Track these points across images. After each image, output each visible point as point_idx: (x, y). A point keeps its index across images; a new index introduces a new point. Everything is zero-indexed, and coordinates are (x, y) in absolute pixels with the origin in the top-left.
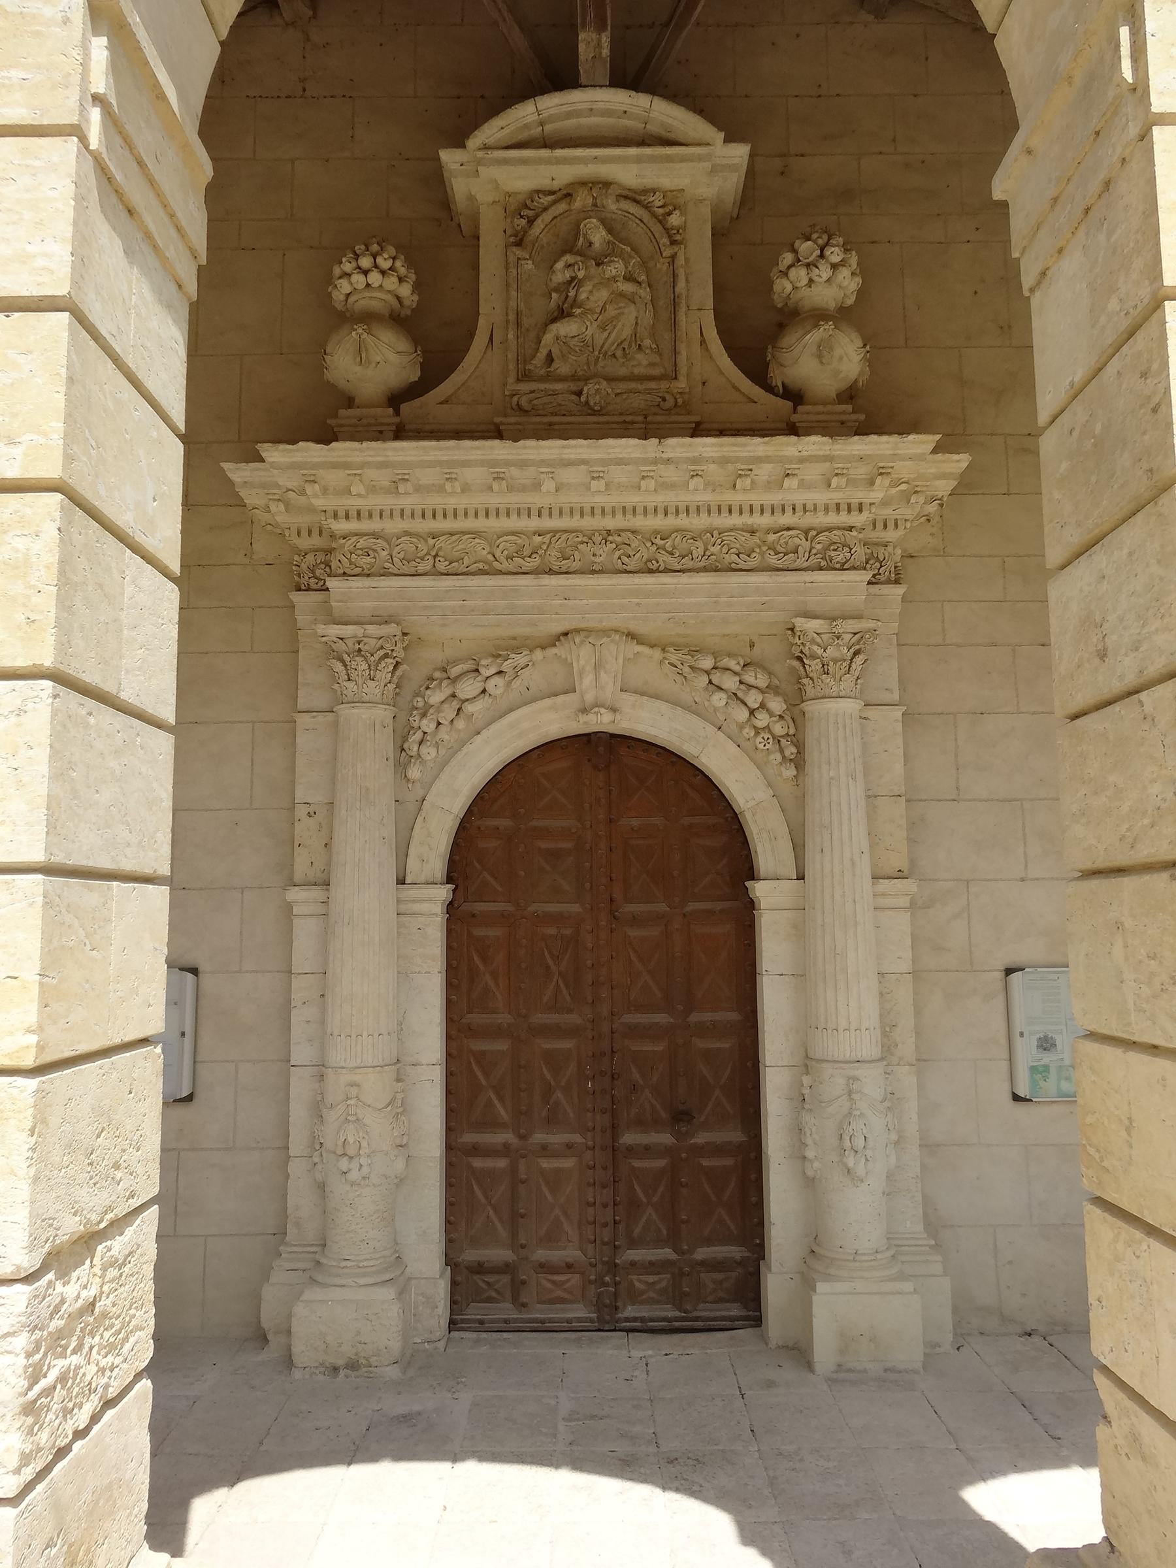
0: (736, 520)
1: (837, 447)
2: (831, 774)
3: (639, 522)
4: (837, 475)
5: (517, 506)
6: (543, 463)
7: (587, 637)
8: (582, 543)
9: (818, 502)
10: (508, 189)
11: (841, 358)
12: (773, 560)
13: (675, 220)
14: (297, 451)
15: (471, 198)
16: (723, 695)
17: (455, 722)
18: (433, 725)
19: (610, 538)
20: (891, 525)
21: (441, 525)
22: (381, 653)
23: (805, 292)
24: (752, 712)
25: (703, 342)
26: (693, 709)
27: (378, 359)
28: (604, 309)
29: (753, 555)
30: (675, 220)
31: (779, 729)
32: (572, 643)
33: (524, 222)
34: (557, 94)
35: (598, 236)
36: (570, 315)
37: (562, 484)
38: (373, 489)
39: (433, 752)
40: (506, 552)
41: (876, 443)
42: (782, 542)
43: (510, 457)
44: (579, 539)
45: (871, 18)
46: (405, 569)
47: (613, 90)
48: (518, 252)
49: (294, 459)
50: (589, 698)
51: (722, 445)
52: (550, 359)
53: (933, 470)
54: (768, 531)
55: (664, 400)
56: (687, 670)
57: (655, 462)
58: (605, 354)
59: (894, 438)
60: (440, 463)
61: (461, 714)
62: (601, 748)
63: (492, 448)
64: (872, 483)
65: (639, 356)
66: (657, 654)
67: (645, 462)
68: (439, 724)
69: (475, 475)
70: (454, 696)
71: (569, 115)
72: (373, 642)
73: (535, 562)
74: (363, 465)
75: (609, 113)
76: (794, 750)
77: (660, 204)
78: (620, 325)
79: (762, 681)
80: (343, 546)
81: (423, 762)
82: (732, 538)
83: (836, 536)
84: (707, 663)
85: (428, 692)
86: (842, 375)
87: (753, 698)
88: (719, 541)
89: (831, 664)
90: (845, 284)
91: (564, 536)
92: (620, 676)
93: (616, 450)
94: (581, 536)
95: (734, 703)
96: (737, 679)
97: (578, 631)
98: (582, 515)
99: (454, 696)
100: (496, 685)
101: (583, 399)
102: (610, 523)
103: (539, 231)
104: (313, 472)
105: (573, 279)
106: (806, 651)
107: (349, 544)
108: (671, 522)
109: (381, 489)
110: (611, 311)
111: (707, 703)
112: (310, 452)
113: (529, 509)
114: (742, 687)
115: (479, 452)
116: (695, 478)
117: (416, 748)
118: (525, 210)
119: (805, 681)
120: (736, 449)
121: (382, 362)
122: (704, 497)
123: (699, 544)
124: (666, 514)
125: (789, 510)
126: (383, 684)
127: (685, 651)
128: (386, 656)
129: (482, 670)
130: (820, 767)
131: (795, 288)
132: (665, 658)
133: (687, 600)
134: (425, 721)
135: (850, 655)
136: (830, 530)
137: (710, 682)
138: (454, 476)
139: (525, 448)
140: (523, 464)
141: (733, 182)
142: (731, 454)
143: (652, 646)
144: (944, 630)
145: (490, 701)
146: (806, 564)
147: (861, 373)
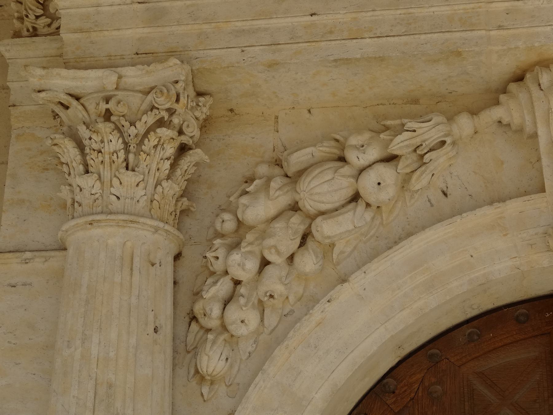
17: (297, 259)
18: (252, 265)
22: (150, 119)
32: (534, 88)
39: (253, 318)
61: (310, 243)
70: (295, 208)
72: (135, 101)
81: (233, 340)
85: (244, 200)
99: (295, 208)
100: (381, 184)
117: (216, 311)
126: (152, 181)
128: (160, 123)
129: (351, 156)
134: (236, 257)
145: (368, 215)
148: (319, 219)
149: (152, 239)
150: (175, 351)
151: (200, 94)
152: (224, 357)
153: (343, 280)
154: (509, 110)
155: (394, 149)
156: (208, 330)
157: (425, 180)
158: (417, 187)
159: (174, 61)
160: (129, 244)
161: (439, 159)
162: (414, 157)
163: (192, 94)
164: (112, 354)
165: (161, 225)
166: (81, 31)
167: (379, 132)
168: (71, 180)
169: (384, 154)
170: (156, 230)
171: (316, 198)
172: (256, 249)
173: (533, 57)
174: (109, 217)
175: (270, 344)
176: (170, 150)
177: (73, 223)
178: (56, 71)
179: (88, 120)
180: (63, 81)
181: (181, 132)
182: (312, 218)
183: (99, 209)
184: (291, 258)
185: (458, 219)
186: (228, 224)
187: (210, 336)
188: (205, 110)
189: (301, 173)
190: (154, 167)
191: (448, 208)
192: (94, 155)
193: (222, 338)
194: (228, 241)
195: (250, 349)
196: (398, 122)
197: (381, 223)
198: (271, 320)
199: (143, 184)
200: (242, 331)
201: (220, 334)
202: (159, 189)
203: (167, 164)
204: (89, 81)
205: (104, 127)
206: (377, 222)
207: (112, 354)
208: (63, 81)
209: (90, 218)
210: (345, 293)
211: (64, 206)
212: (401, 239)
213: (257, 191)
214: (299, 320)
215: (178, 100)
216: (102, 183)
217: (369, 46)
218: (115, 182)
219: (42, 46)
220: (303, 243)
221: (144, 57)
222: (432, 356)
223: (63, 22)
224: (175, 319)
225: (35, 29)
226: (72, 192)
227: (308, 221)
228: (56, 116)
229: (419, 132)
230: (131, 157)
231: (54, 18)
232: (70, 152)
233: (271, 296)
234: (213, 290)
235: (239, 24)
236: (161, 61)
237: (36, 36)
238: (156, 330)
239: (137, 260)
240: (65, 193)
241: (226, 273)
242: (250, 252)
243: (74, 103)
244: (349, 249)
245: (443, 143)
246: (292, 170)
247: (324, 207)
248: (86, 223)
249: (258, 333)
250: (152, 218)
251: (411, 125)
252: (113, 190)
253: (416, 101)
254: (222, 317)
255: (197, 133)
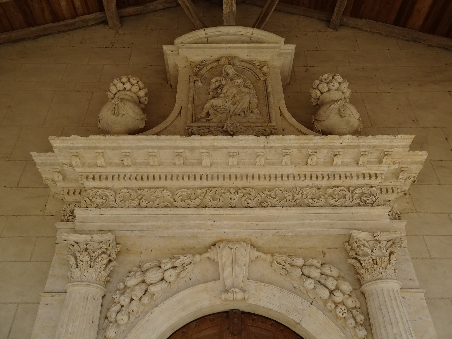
0: (308, 182)
1: (360, 141)
2: (395, 331)
3: (256, 183)
4: (362, 155)
5: (188, 174)
6: (203, 148)
7: (227, 244)
8: (224, 193)
9: (352, 173)
10: (192, 60)
11: (350, 115)
12: (332, 201)
13: (265, 69)
14: (70, 140)
15: (176, 66)
16: (311, 281)
17: (142, 299)
18: (128, 300)
19: (240, 191)
20: (390, 191)
21: (146, 183)
22: (100, 251)
23: (326, 95)
24: (331, 292)
25: (281, 113)
26: (294, 290)
27: (124, 113)
28: (234, 96)
29: (321, 199)
30: (265, 69)
31: (350, 303)
32: (218, 248)
33: (198, 69)
34: (214, 28)
35: (231, 71)
36: (219, 97)
37: (213, 162)
38: (110, 164)
39: (126, 318)
40: (181, 197)
41: (382, 139)
42: (336, 193)
43: (185, 145)
44: (223, 191)
45: (332, 30)
46: (122, 205)
47: (237, 27)
48: (195, 78)
49: (67, 145)
50: (229, 282)
51: (299, 140)
52: (208, 114)
53: (409, 160)
54: (327, 188)
55: (265, 130)
56: (288, 266)
57: (264, 148)
58: (235, 114)
59: (390, 137)
60: (147, 148)
61: (147, 293)
62: (236, 320)
63: (176, 140)
64: (380, 162)
65: (252, 115)
66: (269, 257)
67: (259, 148)
68: (132, 300)
69: (166, 155)
70: (143, 282)
71: (218, 35)
72: (96, 245)
73: (197, 202)
74: (104, 148)
75: (236, 35)
76: (363, 317)
77: (258, 64)
78: (242, 103)
79: (335, 273)
80: (89, 194)
81: (118, 326)
82: (308, 191)
83: (365, 190)
84: (300, 262)
85: (127, 279)
86: (351, 124)
87: (331, 282)
88: (301, 192)
89: (378, 258)
90: (345, 90)
91: (214, 190)
92: (247, 269)
93: (243, 142)
94: (223, 190)
95: (319, 286)
96: (319, 271)
97: (222, 241)
98: (224, 179)
99: (143, 282)
100: (171, 275)
101: (224, 129)
102: (239, 183)
103: (204, 72)
104: (77, 151)
105: (220, 86)
106: (360, 252)
107: (92, 193)
108: (273, 183)
109: (114, 164)
110: (238, 97)
111: (302, 288)
112: (77, 141)
113: (195, 175)
114: (323, 276)
115: (169, 142)
116: (286, 156)
117: (114, 316)
118: (197, 70)
119: (363, 271)
120: (307, 141)
121: (125, 115)
122: (290, 170)
123: (290, 194)
124: (270, 179)
125: (337, 177)
126: (98, 272)
127: (286, 255)
128: (103, 253)
129: (163, 266)
130: (385, 327)
131: (322, 93)
132: (274, 260)
133: (286, 223)
134: (123, 297)
135: (388, 253)
136: (361, 187)
137: (303, 274)
138: (154, 154)
139: (194, 140)
140: (192, 149)
141: (290, 58)
142: (305, 145)
143: (266, 253)
144: (428, 251)
145: (166, 285)
146: (351, 204)
147: (359, 126)
148: (151, 286)
149: (96, 291)
150: (99, 329)
151: (117, 244)
152: (115, 332)
153: (157, 306)
154: (211, 254)
155: (176, 264)
156: (111, 322)
157: (185, 274)
158: (182, 277)
159: (110, 234)
160: (87, 292)
161: (190, 268)
162: (182, 267)
163: (115, 243)
164: (76, 331)
165: (99, 286)
166: (82, 222)
167: (171, 259)
168: (71, 270)
169: (172, 266)
170: (97, 288)
171: (150, 279)
172: (129, 295)
173: (218, 239)
174: (83, 283)
175: (131, 326)
176: (105, 262)
177: (70, 284)
178: (71, 234)
179: (80, 250)
180: (73, 237)
181: (110, 256)
182: (149, 285)
183: (79, 280)
184: (141, 298)
185: (193, 287)
186: (122, 286)
187: (111, 324)
188: (118, 249)
189: (146, 270)
190: (99, 267)
191: (191, 283)
192: (80, 262)
193: (115, 325)
194: (121, 292)
195: (124, 329)
196: (178, 256)
197: (170, 288)
198: (132, 319)
199: (95, 273)
200: (122, 323)
201: (115, 323)
202: (100, 274)
203: (104, 266)
204: (82, 238)
205: (85, 253)
206: (169, 287)
207: (76, 331)
208: (73, 237)
209: (75, 283)
210: (156, 310)
211: (68, 277)
212: (176, 293)
213: (132, 276)
214: (141, 319)
215: (109, 246)
216: (81, 272)
217: (170, 233)
218: (86, 271)
219: (69, 225)
220: (145, 293)
221: (101, 231)
222: (183, 332)
223: (76, 219)
224: (100, 317)
225: (68, 219)
226: (71, 274)
227: (147, 286)
228: (70, 248)
229: (184, 259)
230: (92, 263)
231: (75, 217)
232: (72, 261)
233: (133, 311)
234: (114, 309)
235: (132, 223)
236: (106, 233)
237: (68, 222)
238: (92, 322)
239: (89, 298)
240: (69, 274)
241: (119, 302)
242: (127, 296)
243: (76, 245)
244: (159, 296)
245: (191, 263)
246: (144, 269)
247: (152, 282)
248: (74, 285)
249: (127, 323)
250: (96, 284)
251: (181, 257)
252: (85, 274)
253: (184, 249)
254: (116, 318)
255: (115, 256)
